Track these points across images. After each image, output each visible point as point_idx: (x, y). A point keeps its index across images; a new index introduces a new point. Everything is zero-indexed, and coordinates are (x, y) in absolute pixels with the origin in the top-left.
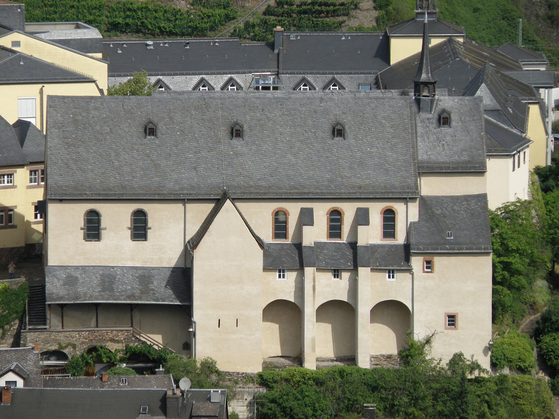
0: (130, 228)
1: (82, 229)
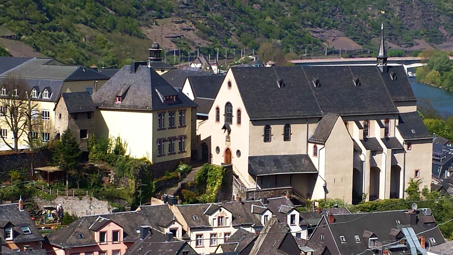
0: (283, 134)
1: (263, 136)
